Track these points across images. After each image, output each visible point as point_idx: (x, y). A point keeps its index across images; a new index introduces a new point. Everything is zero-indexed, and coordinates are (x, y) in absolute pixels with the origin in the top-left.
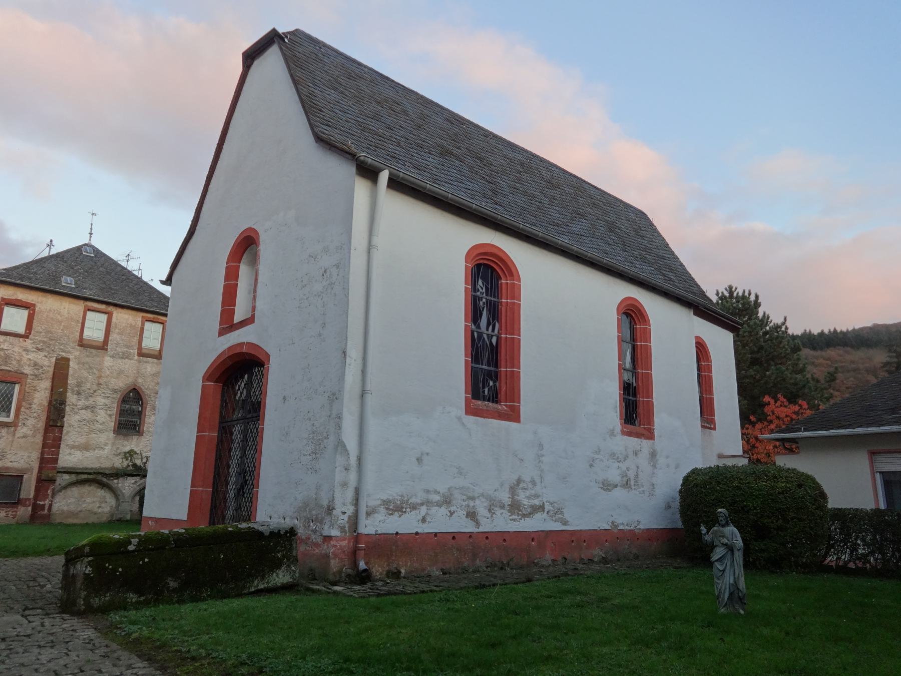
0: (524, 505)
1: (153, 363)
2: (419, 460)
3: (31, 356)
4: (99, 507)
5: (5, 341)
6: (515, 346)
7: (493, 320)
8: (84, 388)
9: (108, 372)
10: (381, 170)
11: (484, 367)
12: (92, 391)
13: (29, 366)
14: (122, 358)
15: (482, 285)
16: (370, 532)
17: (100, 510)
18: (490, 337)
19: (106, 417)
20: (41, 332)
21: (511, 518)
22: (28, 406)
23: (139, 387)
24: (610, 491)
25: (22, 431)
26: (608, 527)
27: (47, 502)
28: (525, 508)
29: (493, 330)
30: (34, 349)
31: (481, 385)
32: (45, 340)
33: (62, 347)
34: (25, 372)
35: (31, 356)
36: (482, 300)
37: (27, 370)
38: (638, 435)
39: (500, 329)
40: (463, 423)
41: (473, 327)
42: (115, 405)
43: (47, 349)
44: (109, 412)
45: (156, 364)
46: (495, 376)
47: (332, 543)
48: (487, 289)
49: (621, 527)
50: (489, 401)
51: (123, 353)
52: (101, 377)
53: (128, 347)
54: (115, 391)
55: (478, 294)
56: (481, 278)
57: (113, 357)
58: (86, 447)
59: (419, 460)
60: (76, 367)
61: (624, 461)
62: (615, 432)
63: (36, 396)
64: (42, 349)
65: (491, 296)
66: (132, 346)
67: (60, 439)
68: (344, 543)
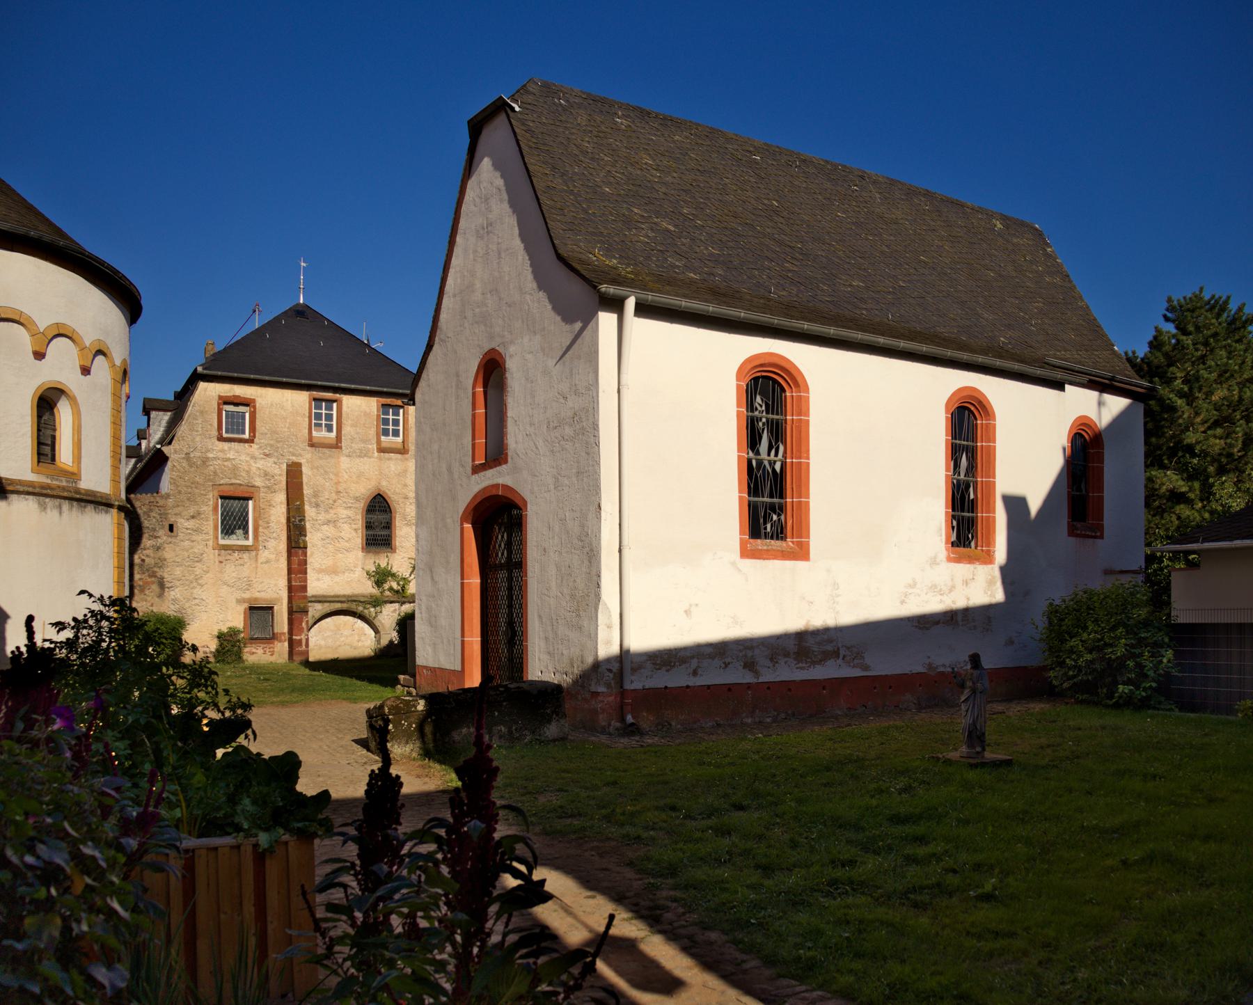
0: (813, 651)
1: (396, 459)
2: (687, 612)
3: (260, 464)
4: (358, 641)
5: (230, 449)
6: (803, 472)
7: (777, 442)
8: (322, 499)
9: (347, 477)
10: (627, 297)
11: (766, 499)
12: (331, 502)
13: (260, 476)
14: (359, 456)
15: (761, 403)
16: (637, 688)
17: (360, 644)
18: (772, 463)
19: (353, 532)
20: (266, 434)
21: (798, 666)
22: (266, 525)
23: (384, 492)
24: (927, 629)
25: (264, 555)
26: (923, 670)
27: (303, 637)
28: (815, 655)
29: (776, 455)
30: (262, 456)
31: (762, 520)
32: (272, 442)
33: (291, 450)
34: (257, 484)
35: (260, 464)
36: (761, 420)
37: (258, 482)
38: (971, 560)
39: (785, 452)
40: (738, 568)
41: (751, 454)
42: (359, 517)
43: (276, 454)
44: (354, 526)
45: (401, 460)
46: (781, 509)
47: (599, 698)
48: (767, 405)
49: (942, 669)
50: (772, 538)
51: (361, 450)
52: (339, 482)
53: (364, 441)
54: (357, 499)
55: (756, 413)
56: (759, 394)
57: (349, 456)
58: (333, 571)
59: (687, 612)
60: (310, 473)
61: (950, 593)
62: (938, 560)
63: (272, 512)
64: (270, 454)
65: (773, 414)
66: (370, 440)
67: (305, 562)
68: (611, 699)
